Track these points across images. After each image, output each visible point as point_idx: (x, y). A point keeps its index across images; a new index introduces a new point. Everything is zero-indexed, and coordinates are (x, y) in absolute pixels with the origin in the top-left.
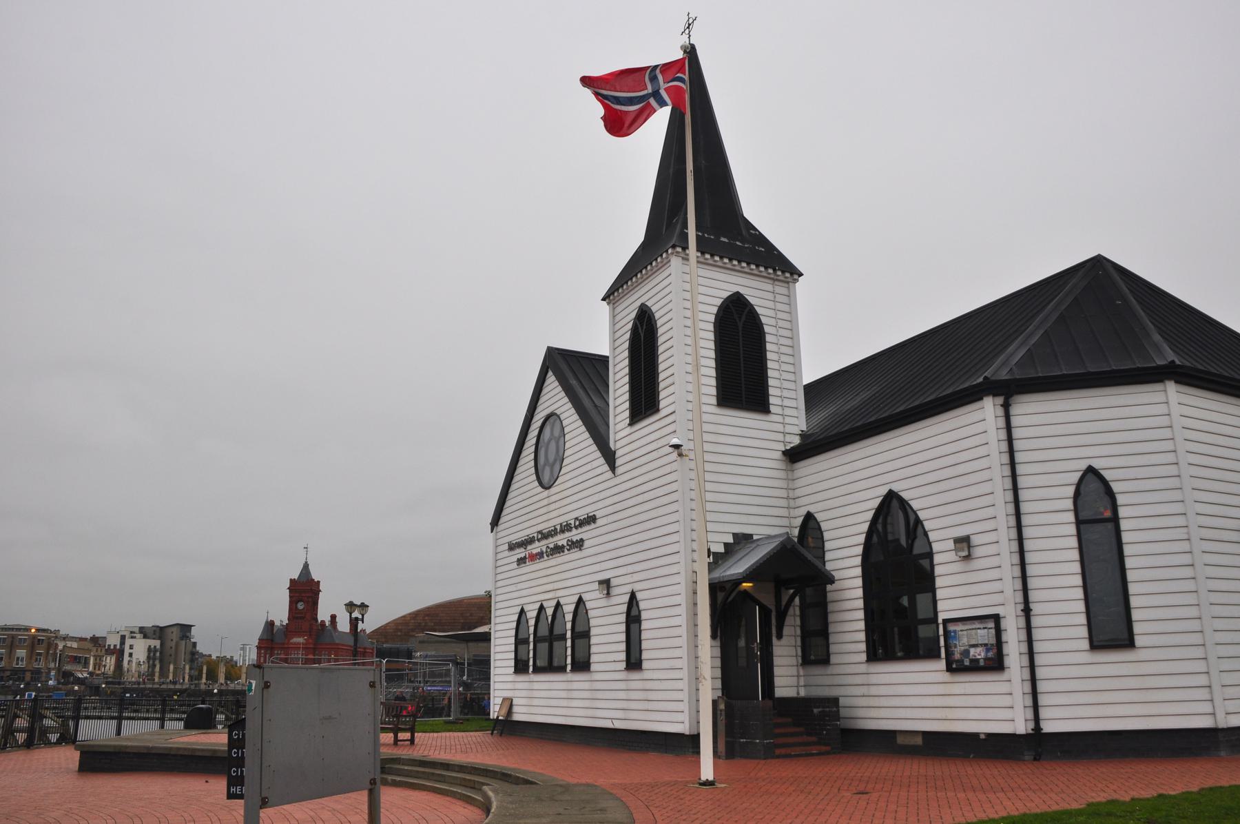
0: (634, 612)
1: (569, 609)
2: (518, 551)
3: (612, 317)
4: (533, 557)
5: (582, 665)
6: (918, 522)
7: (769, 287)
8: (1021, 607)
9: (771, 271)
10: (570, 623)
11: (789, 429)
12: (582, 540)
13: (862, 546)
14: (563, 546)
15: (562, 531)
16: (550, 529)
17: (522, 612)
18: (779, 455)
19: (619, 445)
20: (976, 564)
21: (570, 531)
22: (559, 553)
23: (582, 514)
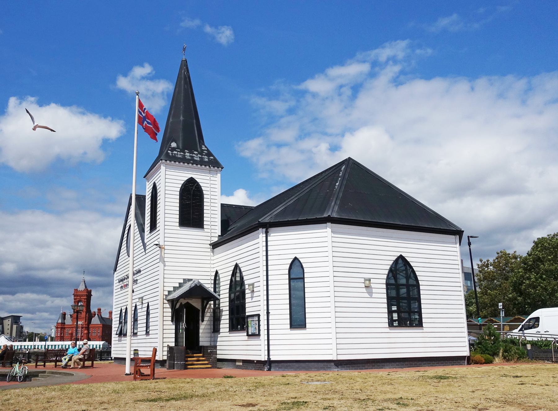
8: (266, 311)
9: (208, 167)
13: (229, 285)
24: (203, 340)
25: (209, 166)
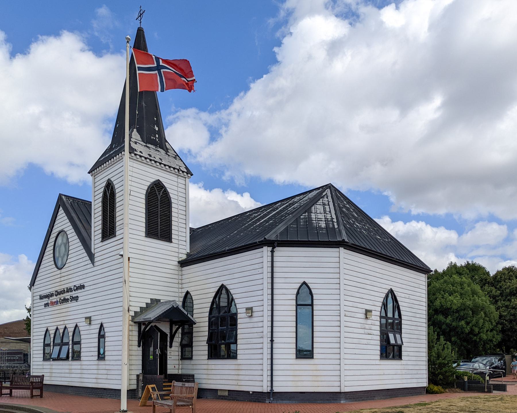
0: (102, 333)
1: (71, 330)
2: (45, 300)
3: (93, 183)
4: (53, 304)
5: (77, 356)
6: (233, 299)
7: (175, 179)
8: (270, 339)
10: (72, 337)
11: (181, 251)
12: (77, 297)
14: (68, 299)
15: (68, 292)
16: (62, 290)
17: (57, 329)
18: (176, 263)
19: (96, 251)
20: (254, 319)
21: (72, 292)
22: (66, 302)
23: (77, 284)
24: (171, 368)
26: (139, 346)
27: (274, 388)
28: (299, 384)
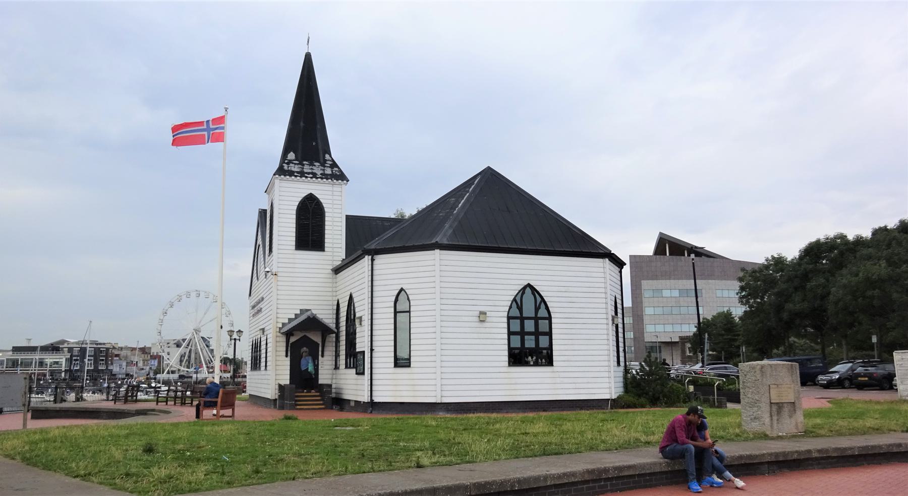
11: (335, 258)
18: (330, 271)
25: (332, 180)
26: (287, 356)
27: (373, 398)
28: (398, 393)
